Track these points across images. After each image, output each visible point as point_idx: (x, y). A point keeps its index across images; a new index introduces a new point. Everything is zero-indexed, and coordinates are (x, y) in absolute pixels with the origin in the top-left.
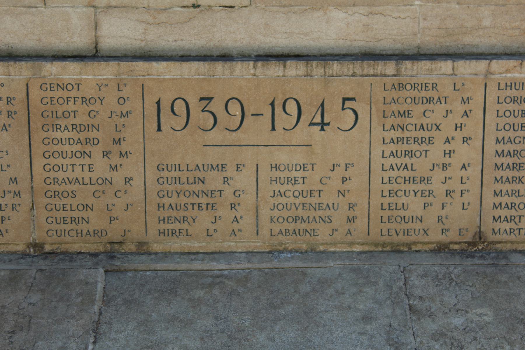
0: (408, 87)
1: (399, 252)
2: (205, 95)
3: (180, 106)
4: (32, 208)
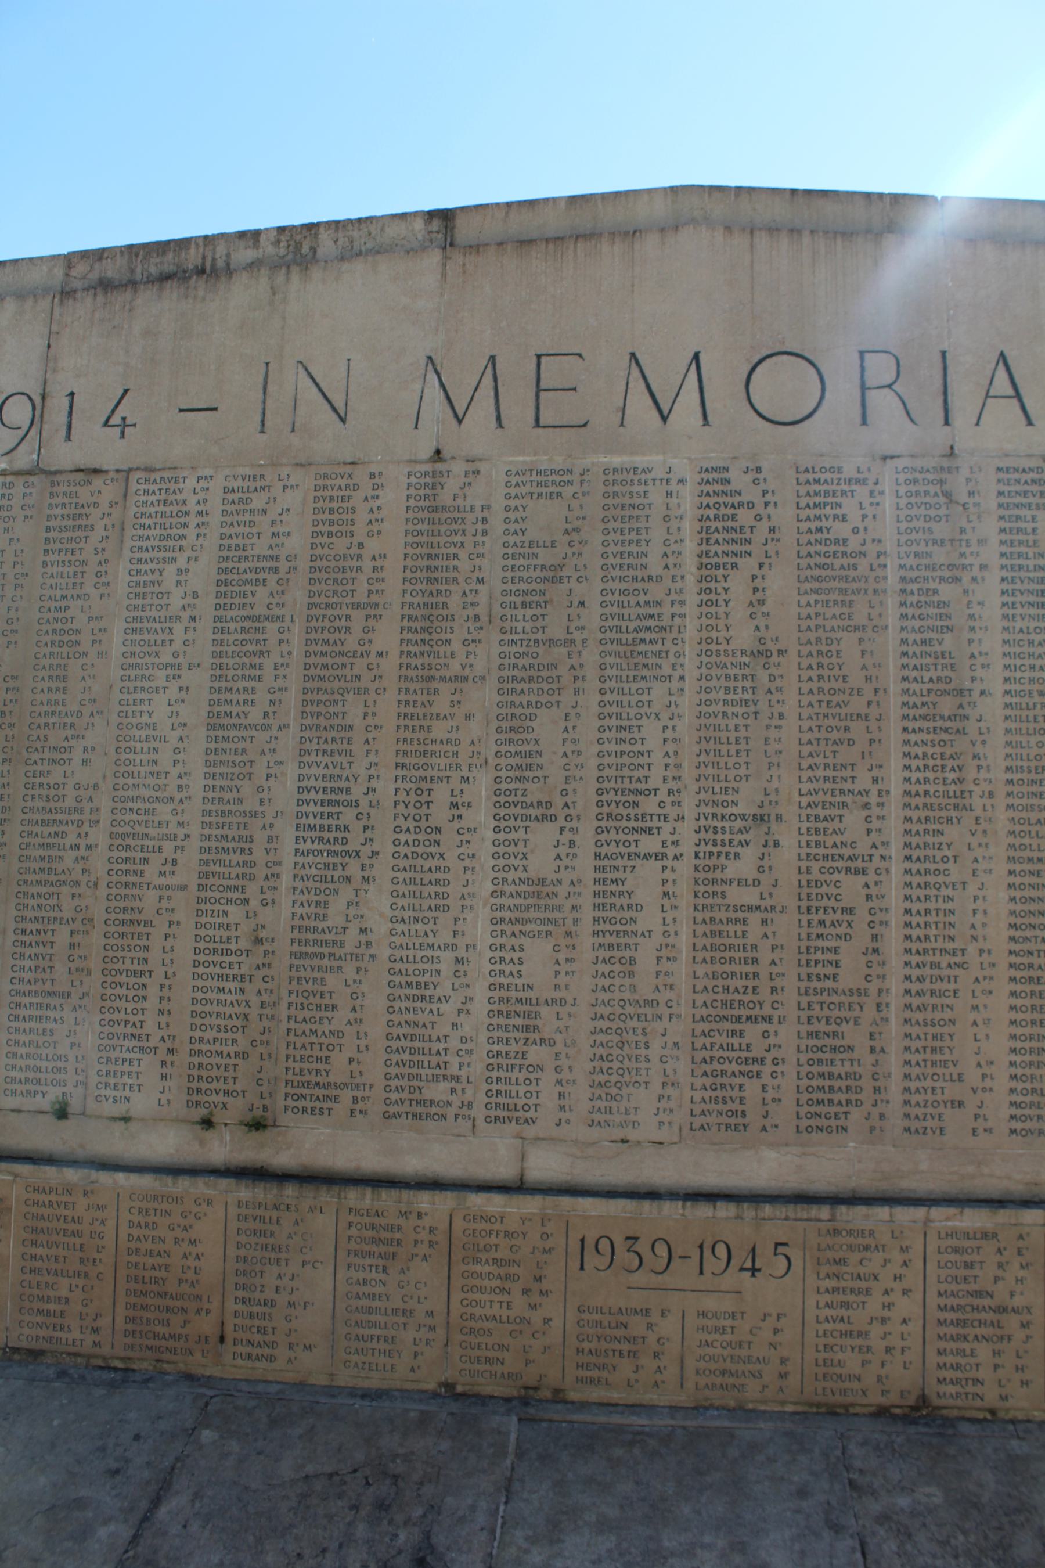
0: (844, 1233)
1: (835, 1414)
2: (631, 1234)
3: (604, 1245)
4: (446, 1345)
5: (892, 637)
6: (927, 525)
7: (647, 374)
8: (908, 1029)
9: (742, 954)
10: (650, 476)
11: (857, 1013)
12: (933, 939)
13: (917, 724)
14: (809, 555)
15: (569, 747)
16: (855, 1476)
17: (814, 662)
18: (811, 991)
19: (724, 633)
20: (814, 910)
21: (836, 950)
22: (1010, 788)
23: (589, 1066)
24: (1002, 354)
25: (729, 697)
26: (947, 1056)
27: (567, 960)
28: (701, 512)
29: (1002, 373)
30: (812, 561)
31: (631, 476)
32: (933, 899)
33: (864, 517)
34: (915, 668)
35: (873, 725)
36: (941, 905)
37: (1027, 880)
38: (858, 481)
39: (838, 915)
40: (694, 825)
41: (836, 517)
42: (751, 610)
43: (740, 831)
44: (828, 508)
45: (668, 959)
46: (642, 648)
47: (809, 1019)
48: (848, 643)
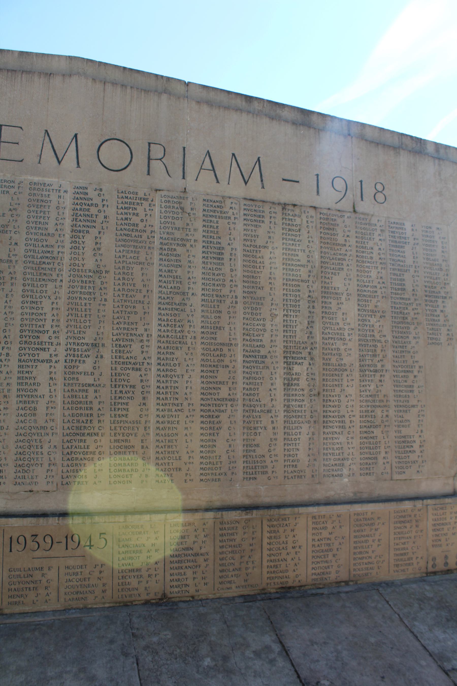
0: (130, 527)
2: (34, 533)
3: (22, 540)
5: (155, 269)
6: (173, 221)
7: (52, 141)
8: (158, 438)
9: (86, 406)
10: (51, 188)
11: (136, 431)
12: (169, 399)
13: (165, 307)
14: (121, 229)
15: (8, 310)
16: (135, 631)
17: (121, 277)
18: (116, 422)
19: (81, 262)
20: (118, 386)
21: (127, 404)
22: (203, 335)
23: (14, 457)
24: (208, 152)
25: (83, 290)
26: (174, 449)
27: (4, 408)
28: (74, 206)
29: (207, 159)
30: (122, 233)
31: (42, 187)
32: (169, 382)
33: (146, 215)
34: (165, 282)
35: (146, 306)
36: (173, 385)
37: (209, 374)
38: (144, 199)
39: (128, 389)
40: (65, 347)
41: (134, 214)
42: (94, 252)
43: (86, 351)
44: (131, 210)
45: (52, 408)
46: (44, 266)
47: (115, 434)
48: (137, 269)
